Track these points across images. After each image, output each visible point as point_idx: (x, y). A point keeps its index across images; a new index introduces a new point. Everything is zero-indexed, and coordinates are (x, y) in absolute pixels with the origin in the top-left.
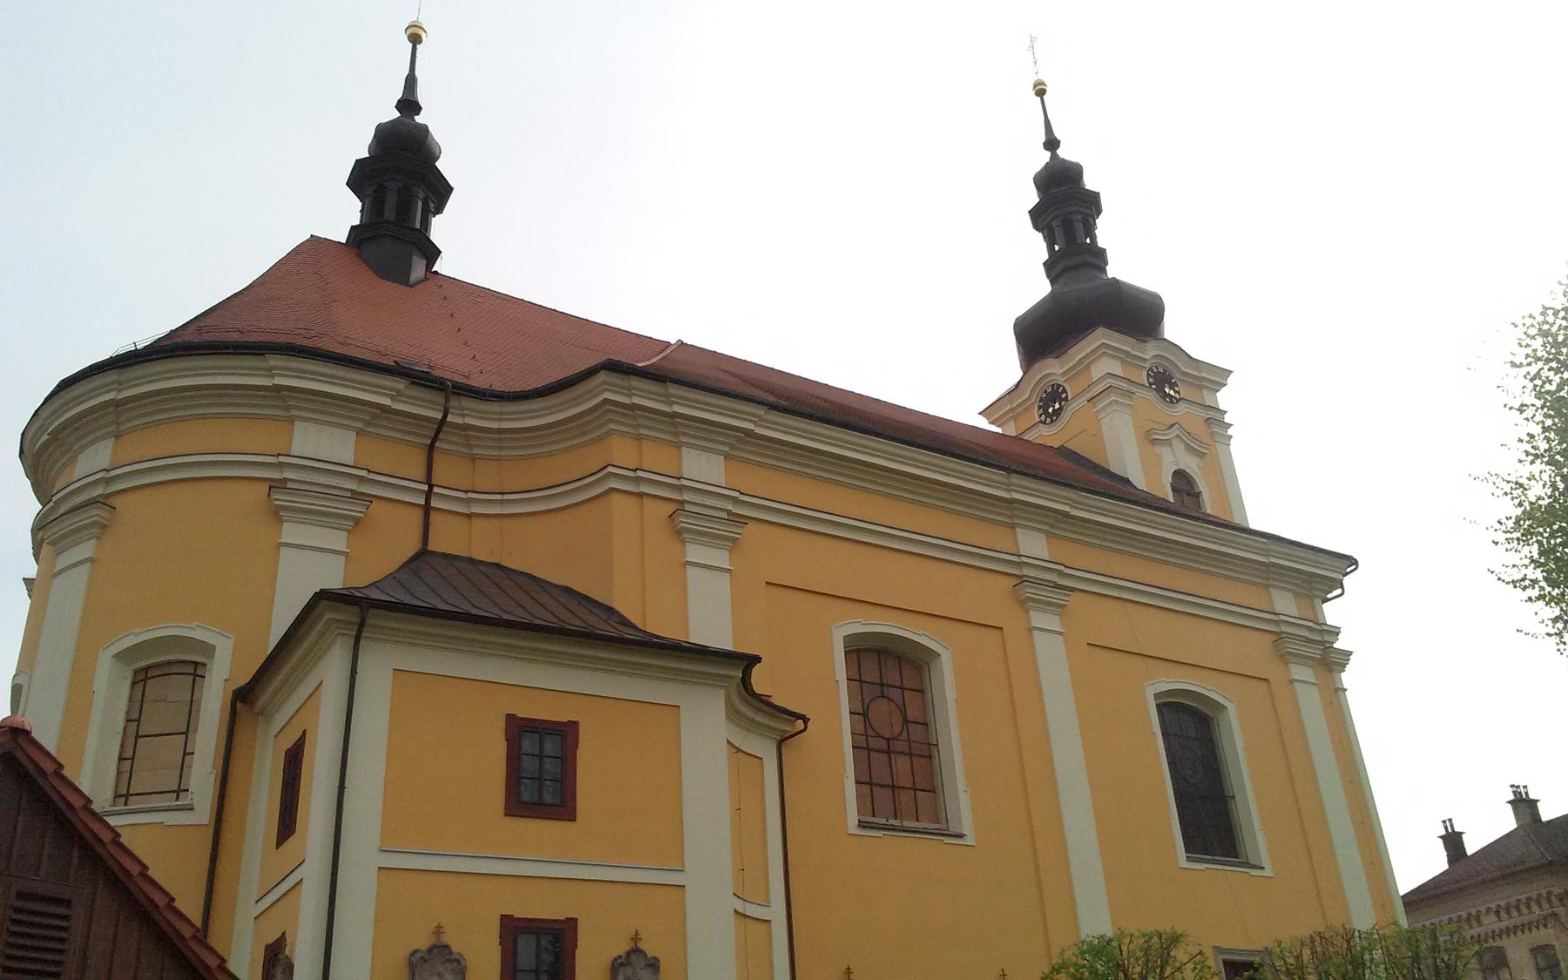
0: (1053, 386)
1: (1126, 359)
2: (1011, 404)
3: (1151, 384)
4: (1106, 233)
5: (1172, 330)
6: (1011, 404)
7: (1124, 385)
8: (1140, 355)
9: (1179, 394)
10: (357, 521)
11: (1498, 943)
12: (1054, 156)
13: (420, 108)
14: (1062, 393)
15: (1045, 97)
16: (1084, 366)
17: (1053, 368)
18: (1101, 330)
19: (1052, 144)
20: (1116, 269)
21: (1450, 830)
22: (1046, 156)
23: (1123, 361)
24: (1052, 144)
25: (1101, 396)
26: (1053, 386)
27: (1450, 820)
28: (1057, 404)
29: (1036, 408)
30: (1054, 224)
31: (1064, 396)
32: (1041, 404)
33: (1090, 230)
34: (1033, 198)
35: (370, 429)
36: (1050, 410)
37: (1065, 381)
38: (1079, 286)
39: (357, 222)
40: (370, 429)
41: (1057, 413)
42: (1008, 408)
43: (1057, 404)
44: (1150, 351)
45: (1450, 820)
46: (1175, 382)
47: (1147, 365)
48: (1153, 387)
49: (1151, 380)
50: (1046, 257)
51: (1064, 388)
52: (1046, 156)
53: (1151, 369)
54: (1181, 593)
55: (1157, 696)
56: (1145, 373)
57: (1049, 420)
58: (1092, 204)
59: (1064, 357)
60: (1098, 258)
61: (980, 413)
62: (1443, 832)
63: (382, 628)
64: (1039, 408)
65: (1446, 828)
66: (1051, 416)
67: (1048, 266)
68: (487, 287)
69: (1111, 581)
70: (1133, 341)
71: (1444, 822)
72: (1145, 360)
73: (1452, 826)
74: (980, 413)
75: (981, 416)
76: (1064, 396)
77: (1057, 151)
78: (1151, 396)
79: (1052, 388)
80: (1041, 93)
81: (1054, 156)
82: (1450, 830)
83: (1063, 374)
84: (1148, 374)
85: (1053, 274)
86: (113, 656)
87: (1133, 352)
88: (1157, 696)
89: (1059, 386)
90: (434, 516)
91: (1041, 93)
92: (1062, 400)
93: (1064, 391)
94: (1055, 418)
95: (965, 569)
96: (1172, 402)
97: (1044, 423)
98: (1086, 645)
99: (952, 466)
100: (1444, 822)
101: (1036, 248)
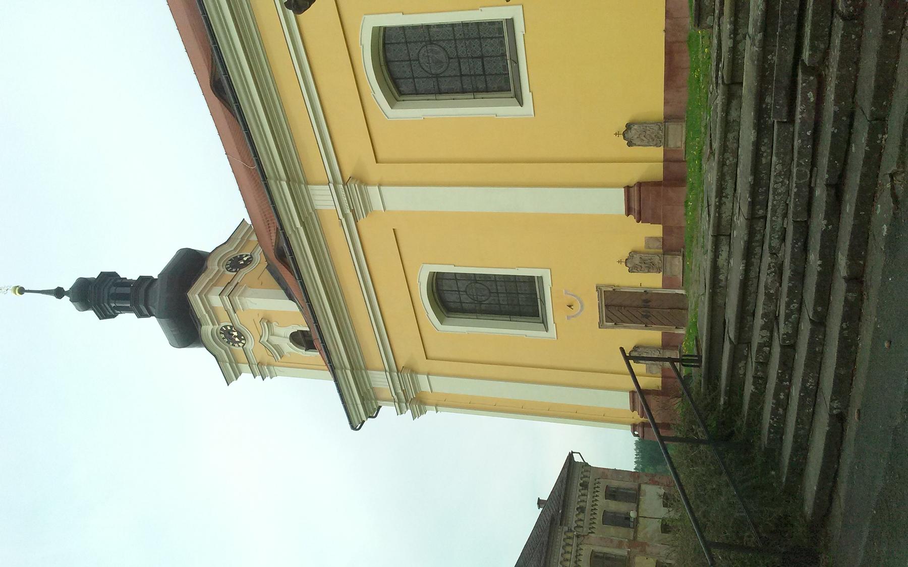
1: (214, 283)
2: (226, 362)
4: (130, 272)
5: (206, 246)
6: (226, 362)
7: (230, 288)
8: (214, 273)
9: (248, 255)
13: (59, 288)
14: (227, 328)
16: (212, 311)
17: (207, 329)
18: (189, 295)
19: (59, 293)
20: (154, 270)
22: (66, 299)
23: (215, 285)
24: (59, 293)
25: (233, 304)
26: (221, 333)
28: (234, 333)
29: (232, 347)
30: (113, 305)
31: (229, 328)
32: (231, 344)
33: (125, 283)
34: (91, 314)
35: (363, 367)
36: (237, 339)
37: (219, 325)
38: (158, 297)
40: (363, 367)
41: (240, 335)
42: (228, 364)
43: (234, 333)
44: (213, 266)
46: (240, 255)
48: (238, 269)
49: (234, 270)
50: (133, 316)
51: (224, 326)
52: (66, 299)
53: (227, 269)
54: (365, 301)
55: (511, 22)
56: (227, 273)
57: (243, 341)
58: (109, 279)
59: (202, 321)
60: (145, 281)
61: (228, 385)
66: (241, 340)
67: (140, 315)
69: (368, 303)
70: (203, 276)
72: (219, 271)
74: (228, 385)
75: (230, 385)
76: (229, 328)
77: (65, 290)
78: (244, 271)
79: (223, 334)
80: (22, 291)
83: (213, 324)
84: (230, 271)
85: (146, 312)
86: (392, 109)
87: (211, 277)
88: (511, 22)
89: (221, 329)
91: (22, 291)
92: (231, 330)
93: (225, 327)
94: (242, 337)
95: (381, 306)
96: (251, 261)
97: (244, 344)
99: (312, 290)
101: (127, 319)
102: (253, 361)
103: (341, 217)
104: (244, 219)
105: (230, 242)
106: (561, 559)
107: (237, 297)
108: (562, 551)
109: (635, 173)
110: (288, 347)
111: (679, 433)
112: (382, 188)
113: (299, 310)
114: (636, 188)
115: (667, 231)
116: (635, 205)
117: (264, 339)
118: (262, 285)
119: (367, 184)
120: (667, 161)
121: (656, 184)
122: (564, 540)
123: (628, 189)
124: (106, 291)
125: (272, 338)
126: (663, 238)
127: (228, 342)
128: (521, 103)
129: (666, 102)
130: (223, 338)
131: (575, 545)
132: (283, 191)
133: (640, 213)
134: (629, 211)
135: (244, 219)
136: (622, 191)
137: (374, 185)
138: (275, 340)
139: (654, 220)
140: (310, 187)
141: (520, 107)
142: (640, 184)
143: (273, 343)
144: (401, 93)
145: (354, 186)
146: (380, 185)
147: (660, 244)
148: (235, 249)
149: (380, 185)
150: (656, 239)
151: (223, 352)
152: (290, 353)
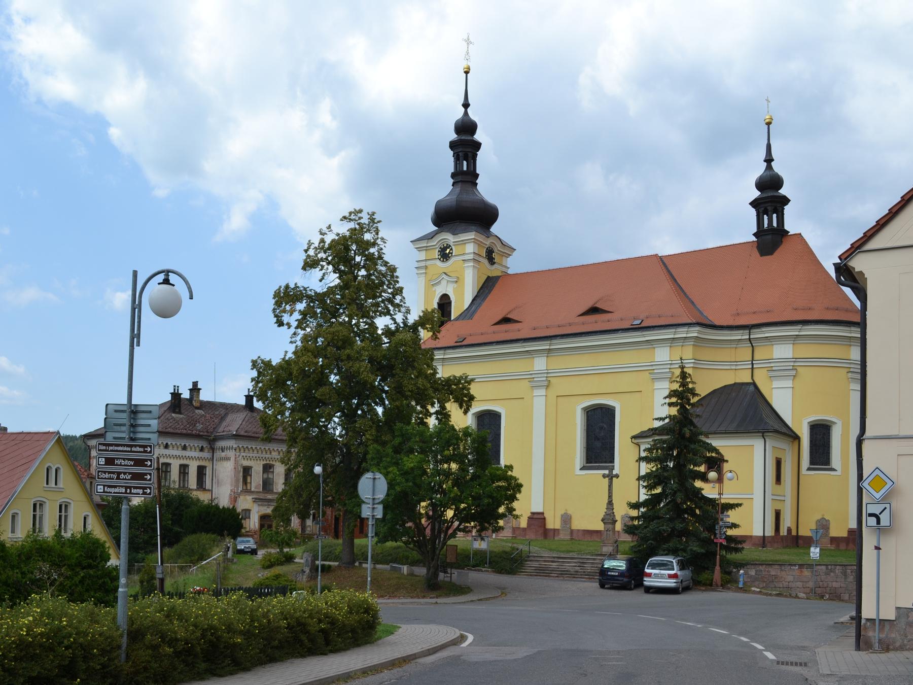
0: (447, 244)
3: (486, 256)
4: (484, 160)
10: (794, 376)
11: (67, 450)
12: (466, 113)
15: (468, 75)
16: (464, 242)
21: (176, 391)
26: (447, 244)
27: (178, 387)
29: (437, 250)
30: (460, 154)
39: (453, 171)
45: (178, 387)
47: (487, 247)
56: (485, 249)
57: (445, 260)
61: (411, 242)
62: (173, 391)
63: (446, 365)
64: (439, 251)
65: (175, 390)
68: (558, 268)
71: (175, 386)
72: (486, 245)
73: (178, 390)
74: (411, 242)
78: (486, 262)
80: (467, 73)
81: (466, 113)
82: (176, 391)
83: (454, 242)
84: (486, 252)
90: (755, 371)
91: (467, 73)
97: (440, 259)
98: (288, 330)
100: (175, 386)
102: (428, 263)
103: (530, 373)
104: (515, 250)
105: (502, 246)
106: (241, 446)
107: (472, 264)
108: (245, 446)
109: (549, 516)
110: (439, 291)
111: (234, 561)
112: (544, 397)
113: (465, 309)
114: (543, 517)
115: (524, 529)
116: (535, 516)
117: (444, 276)
118: (479, 277)
119: (546, 389)
120: (555, 530)
121: (545, 525)
122: (243, 447)
123: (543, 513)
124: (470, 150)
125: (446, 281)
126: (519, 528)
127: (440, 248)
128: (581, 469)
129: (578, 530)
130: (443, 245)
131: (262, 455)
132: (544, 346)
133: (532, 518)
134: (533, 513)
135: (515, 250)
136: (541, 511)
137: (546, 393)
138: (444, 283)
139: (528, 524)
140: (545, 358)
141: (579, 468)
142: (544, 519)
143: (441, 281)
144: (587, 412)
145: (546, 383)
146: (546, 396)
147: (517, 526)
148: (498, 250)
149: (546, 396)
150: (519, 525)
151: (435, 244)
152: (435, 291)
